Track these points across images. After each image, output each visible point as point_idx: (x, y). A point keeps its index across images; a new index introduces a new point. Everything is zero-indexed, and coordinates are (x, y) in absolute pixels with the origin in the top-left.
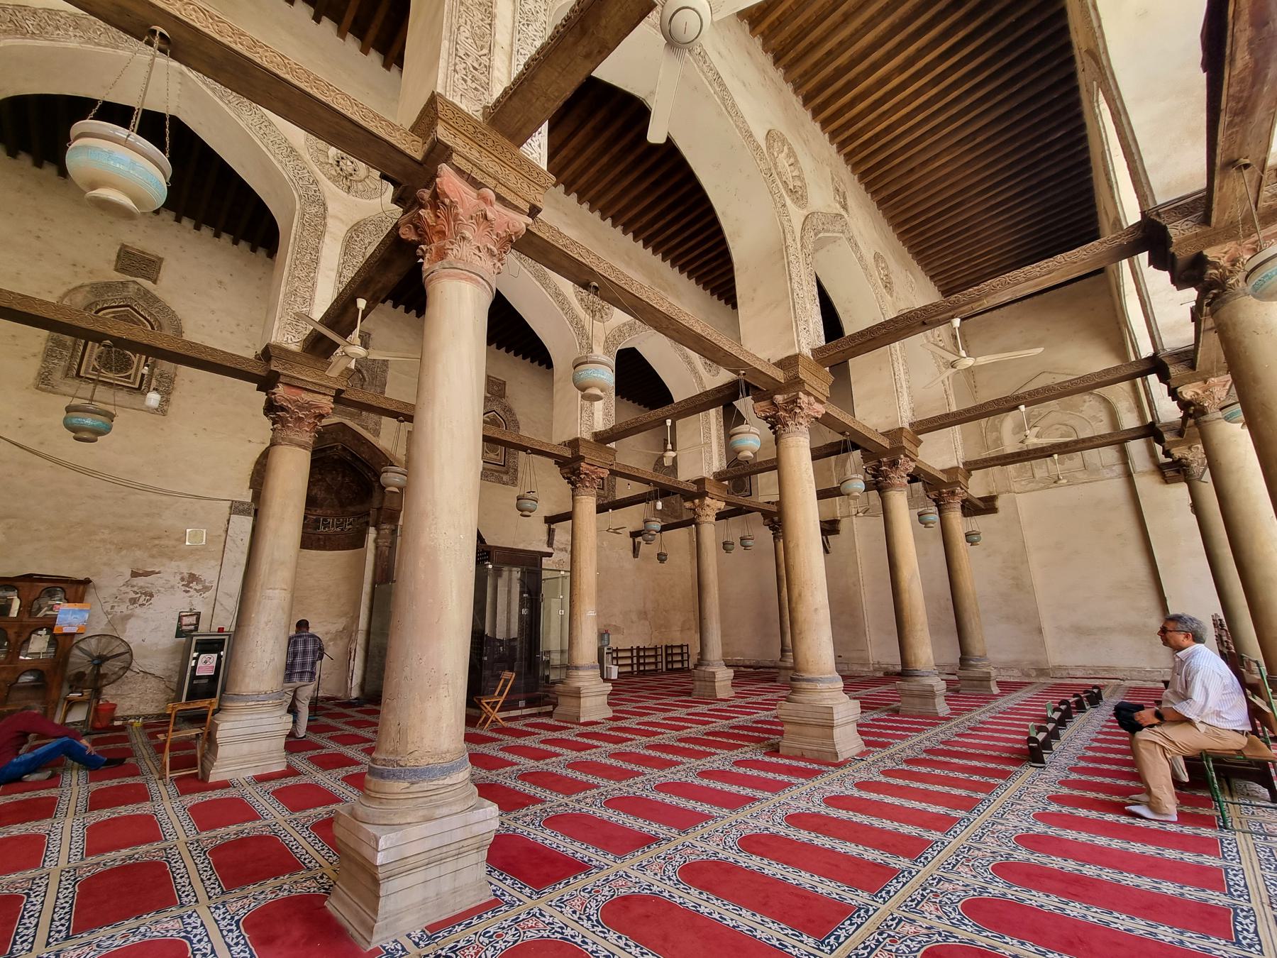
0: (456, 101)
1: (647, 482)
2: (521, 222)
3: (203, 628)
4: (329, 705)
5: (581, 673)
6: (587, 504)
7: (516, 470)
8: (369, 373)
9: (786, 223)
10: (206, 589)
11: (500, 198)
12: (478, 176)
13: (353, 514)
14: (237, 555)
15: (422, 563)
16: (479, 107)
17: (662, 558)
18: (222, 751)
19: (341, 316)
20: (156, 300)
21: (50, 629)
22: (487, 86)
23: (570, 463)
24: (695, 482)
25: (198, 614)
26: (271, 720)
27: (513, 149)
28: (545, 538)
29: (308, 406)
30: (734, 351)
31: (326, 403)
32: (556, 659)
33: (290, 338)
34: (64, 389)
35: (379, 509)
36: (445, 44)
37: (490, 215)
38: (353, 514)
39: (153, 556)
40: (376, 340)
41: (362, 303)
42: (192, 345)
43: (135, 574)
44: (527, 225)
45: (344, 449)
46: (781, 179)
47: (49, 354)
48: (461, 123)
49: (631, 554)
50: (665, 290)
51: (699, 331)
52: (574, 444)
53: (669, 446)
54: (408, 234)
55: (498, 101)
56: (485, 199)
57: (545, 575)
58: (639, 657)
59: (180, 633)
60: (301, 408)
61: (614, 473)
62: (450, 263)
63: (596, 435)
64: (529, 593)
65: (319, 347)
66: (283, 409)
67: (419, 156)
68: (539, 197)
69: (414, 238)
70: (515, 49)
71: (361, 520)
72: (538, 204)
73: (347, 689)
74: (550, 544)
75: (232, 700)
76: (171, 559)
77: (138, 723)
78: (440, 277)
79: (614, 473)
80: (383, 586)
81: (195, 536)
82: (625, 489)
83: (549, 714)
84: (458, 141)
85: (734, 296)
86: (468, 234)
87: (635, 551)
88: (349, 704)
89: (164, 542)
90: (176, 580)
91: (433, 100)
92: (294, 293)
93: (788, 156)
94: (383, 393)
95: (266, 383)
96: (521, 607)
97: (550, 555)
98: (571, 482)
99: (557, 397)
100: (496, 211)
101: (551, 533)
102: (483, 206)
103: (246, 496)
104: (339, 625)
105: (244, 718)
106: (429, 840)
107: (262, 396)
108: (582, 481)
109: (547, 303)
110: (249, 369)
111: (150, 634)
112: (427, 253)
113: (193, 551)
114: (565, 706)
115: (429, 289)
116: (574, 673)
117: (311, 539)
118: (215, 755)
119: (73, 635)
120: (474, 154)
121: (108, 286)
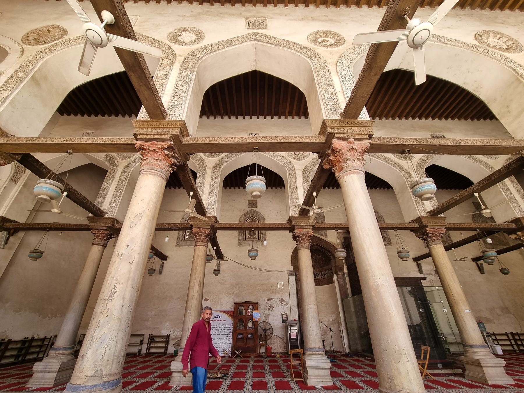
0: (331, 118)
1: (474, 229)
2: (367, 143)
3: (289, 319)
4: (338, 355)
5: (475, 350)
6: (438, 249)
7: (389, 238)
8: (320, 216)
9: (513, 66)
10: (287, 304)
11: (356, 139)
12: (346, 136)
13: (326, 270)
14: (293, 291)
15: (373, 294)
16: (339, 115)
17: (504, 272)
18: (310, 372)
19: (309, 201)
20: (258, 212)
21: (252, 319)
22: (339, 107)
23: (420, 229)
24: (512, 222)
25: (287, 314)
26: (323, 361)
27: (355, 120)
28: (416, 269)
29: (305, 234)
30: (511, 143)
31: (310, 231)
32: (450, 339)
33: (295, 213)
34: (244, 244)
35: (335, 266)
36: (322, 104)
37: (354, 147)
38: (326, 270)
39: (271, 293)
40: (325, 206)
41: (314, 194)
42: (271, 224)
43: (268, 300)
44: (370, 143)
45: (317, 245)
46: (496, 48)
47: (239, 236)
48: (334, 123)
49: (478, 272)
50: (441, 132)
51: (479, 144)
52: (418, 220)
53: (483, 207)
54: (326, 166)
55: (345, 109)
56: (351, 143)
57: (426, 289)
58: (516, 340)
59: (283, 321)
60: (303, 235)
61: (448, 229)
62: (345, 170)
63: (429, 213)
64: (420, 300)
65: (304, 212)
66: (298, 237)
67: (324, 141)
68: (370, 131)
69: (329, 167)
70: (344, 89)
71: (330, 272)
72: (371, 133)
73: (343, 348)
74: (421, 271)
75: (308, 350)
76: (276, 294)
77: (278, 355)
78: (343, 176)
79: (448, 229)
80: (346, 300)
81: (281, 285)
82: (457, 236)
83: (462, 375)
84: (336, 129)
85: (491, 113)
86: (348, 157)
87: (481, 269)
88: (346, 355)
89: (273, 288)
90: (278, 301)
91: (324, 122)
92: (293, 198)
93: (495, 36)
94: (324, 221)
95: (291, 229)
96: (418, 308)
97: (425, 278)
98: (423, 239)
99: (400, 201)
100: (357, 145)
101: (419, 266)
102: (351, 145)
103: (291, 268)
104: (332, 318)
105: (313, 359)
106: (179, 375)
107: (291, 234)
108: (430, 237)
109: (383, 166)
110: (286, 226)
111: (275, 321)
112: (336, 169)
113: (281, 290)
114: (471, 371)
115: (340, 182)
116: (470, 349)
117: (317, 283)
118: (307, 373)
119: (257, 321)
120: (342, 130)
121: (247, 213)
